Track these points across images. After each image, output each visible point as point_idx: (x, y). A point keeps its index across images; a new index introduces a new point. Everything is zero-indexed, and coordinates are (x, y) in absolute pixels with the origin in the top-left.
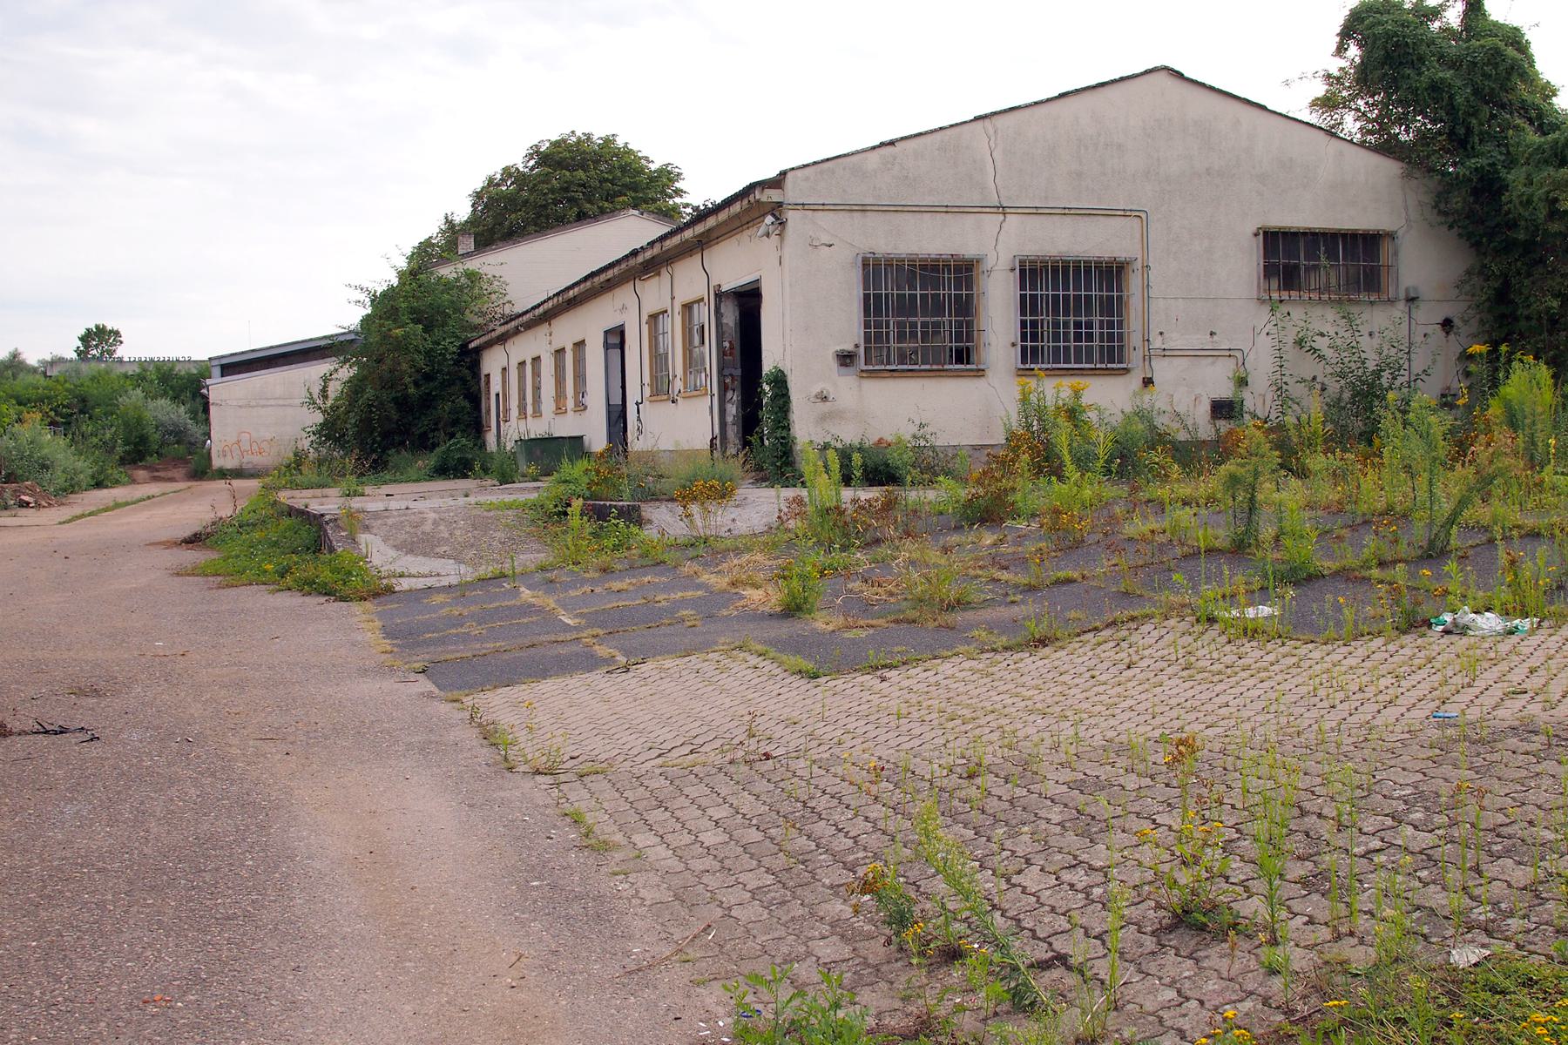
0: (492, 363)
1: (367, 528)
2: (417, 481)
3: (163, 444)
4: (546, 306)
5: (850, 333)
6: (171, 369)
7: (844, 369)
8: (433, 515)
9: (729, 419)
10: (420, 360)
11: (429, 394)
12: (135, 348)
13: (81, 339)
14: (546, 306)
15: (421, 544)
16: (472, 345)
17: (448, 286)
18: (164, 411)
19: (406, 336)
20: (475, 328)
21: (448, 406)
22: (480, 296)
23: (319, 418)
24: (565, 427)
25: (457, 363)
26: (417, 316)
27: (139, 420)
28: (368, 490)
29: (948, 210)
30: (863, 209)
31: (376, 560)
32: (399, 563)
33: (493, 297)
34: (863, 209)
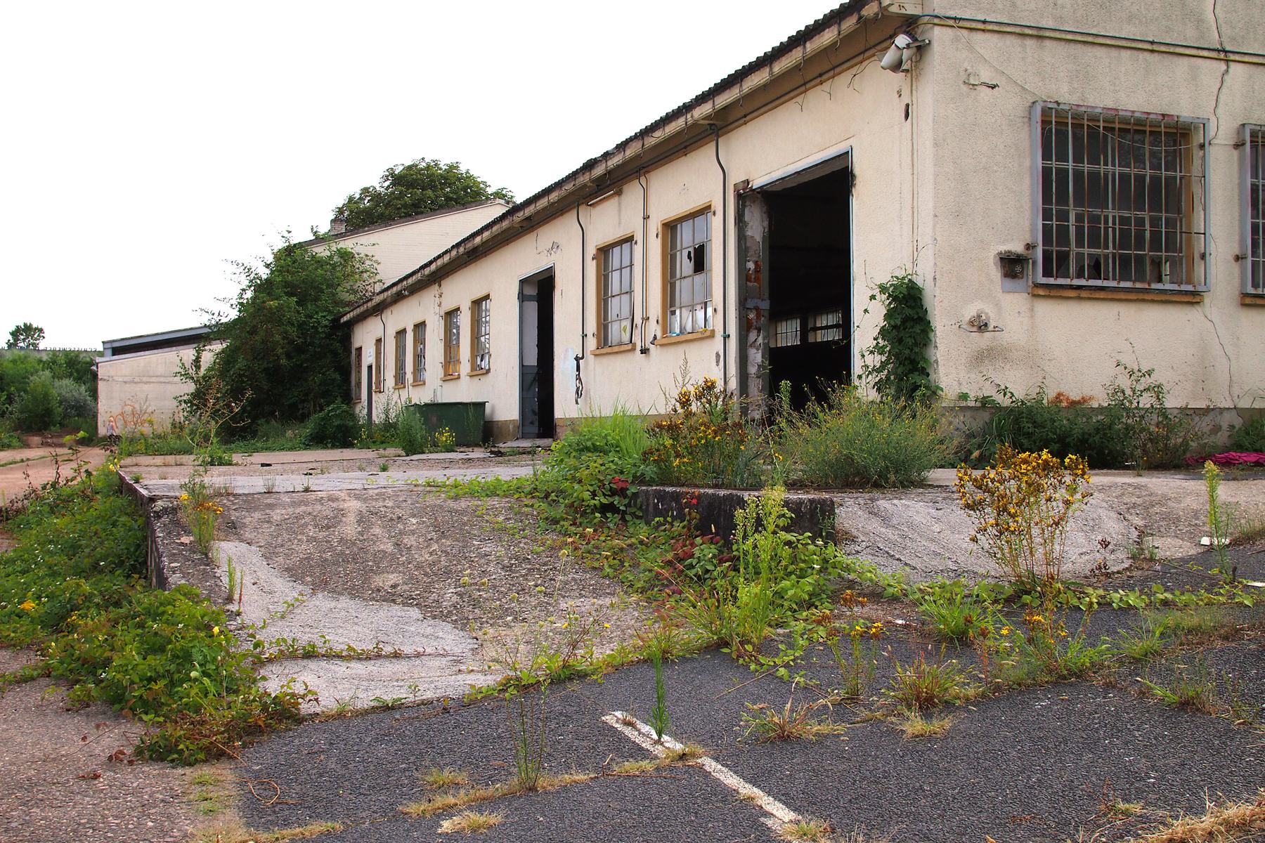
0: (366, 337)
1: (233, 529)
2: (291, 449)
3: (66, 416)
4: (440, 262)
5: (1016, 220)
6: (77, 356)
7: (1010, 283)
8: (353, 505)
9: (753, 370)
10: (293, 332)
11: (301, 365)
12: (54, 340)
13: (12, 334)
14: (440, 262)
15: (336, 568)
16: (345, 319)
17: (320, 262)
18: (67, 388)
19: (280, 308)
20: (349, 304)
21: (318, 378)
22: (353, 273)
23: (191, 387)
24: (463, 391)
25: (328, 336)
26: (290, 289)
27: (46, 395)
28: (236, 458)
29: (1154, 48)
30: (1039, 35)
31: (252, 609)
32: (302, 615)
33: (365, 275)
34: (1039, 35)
